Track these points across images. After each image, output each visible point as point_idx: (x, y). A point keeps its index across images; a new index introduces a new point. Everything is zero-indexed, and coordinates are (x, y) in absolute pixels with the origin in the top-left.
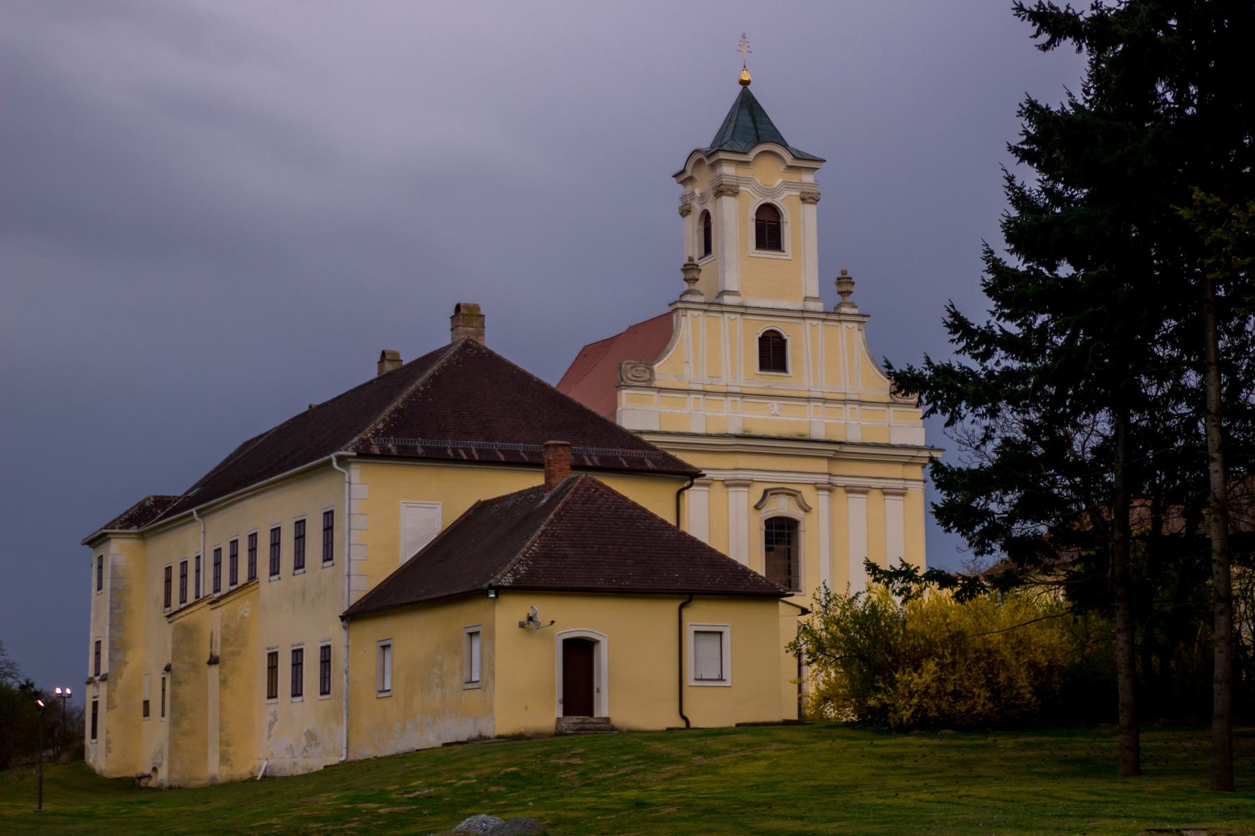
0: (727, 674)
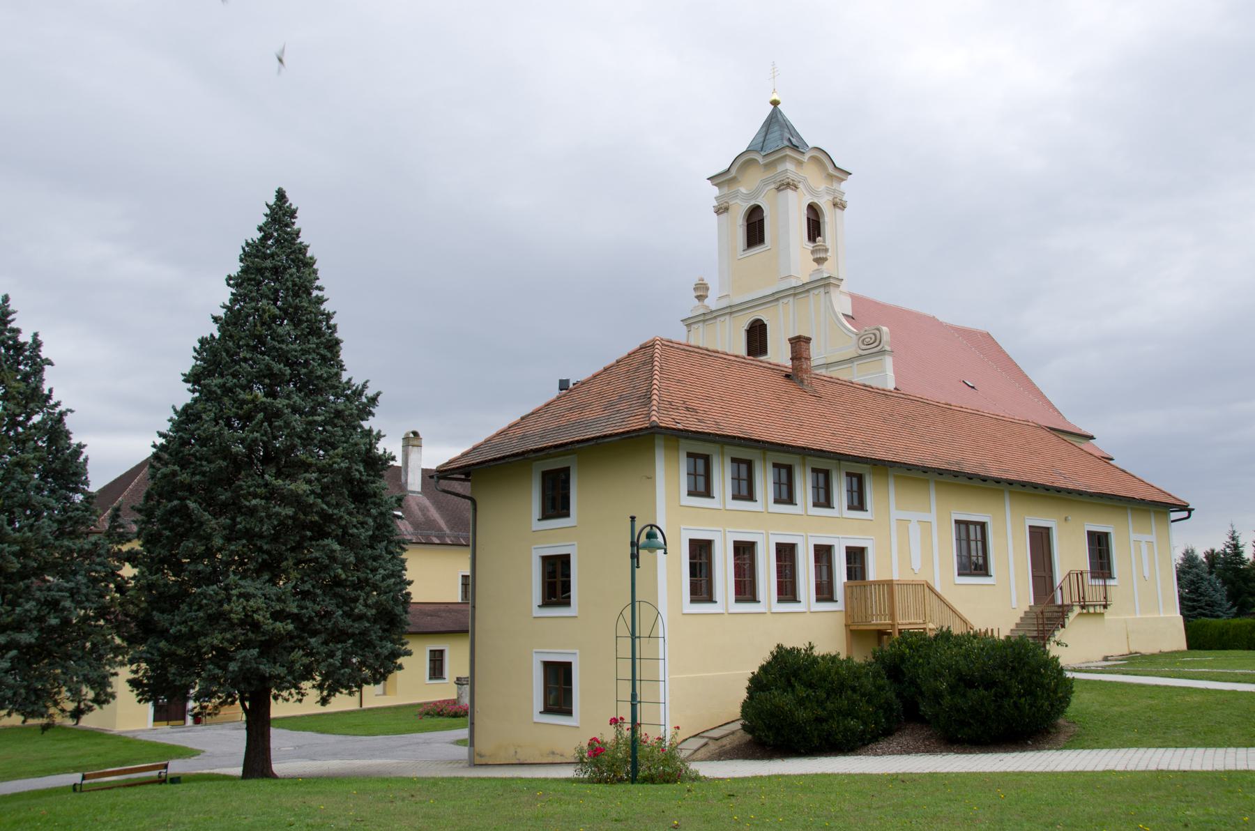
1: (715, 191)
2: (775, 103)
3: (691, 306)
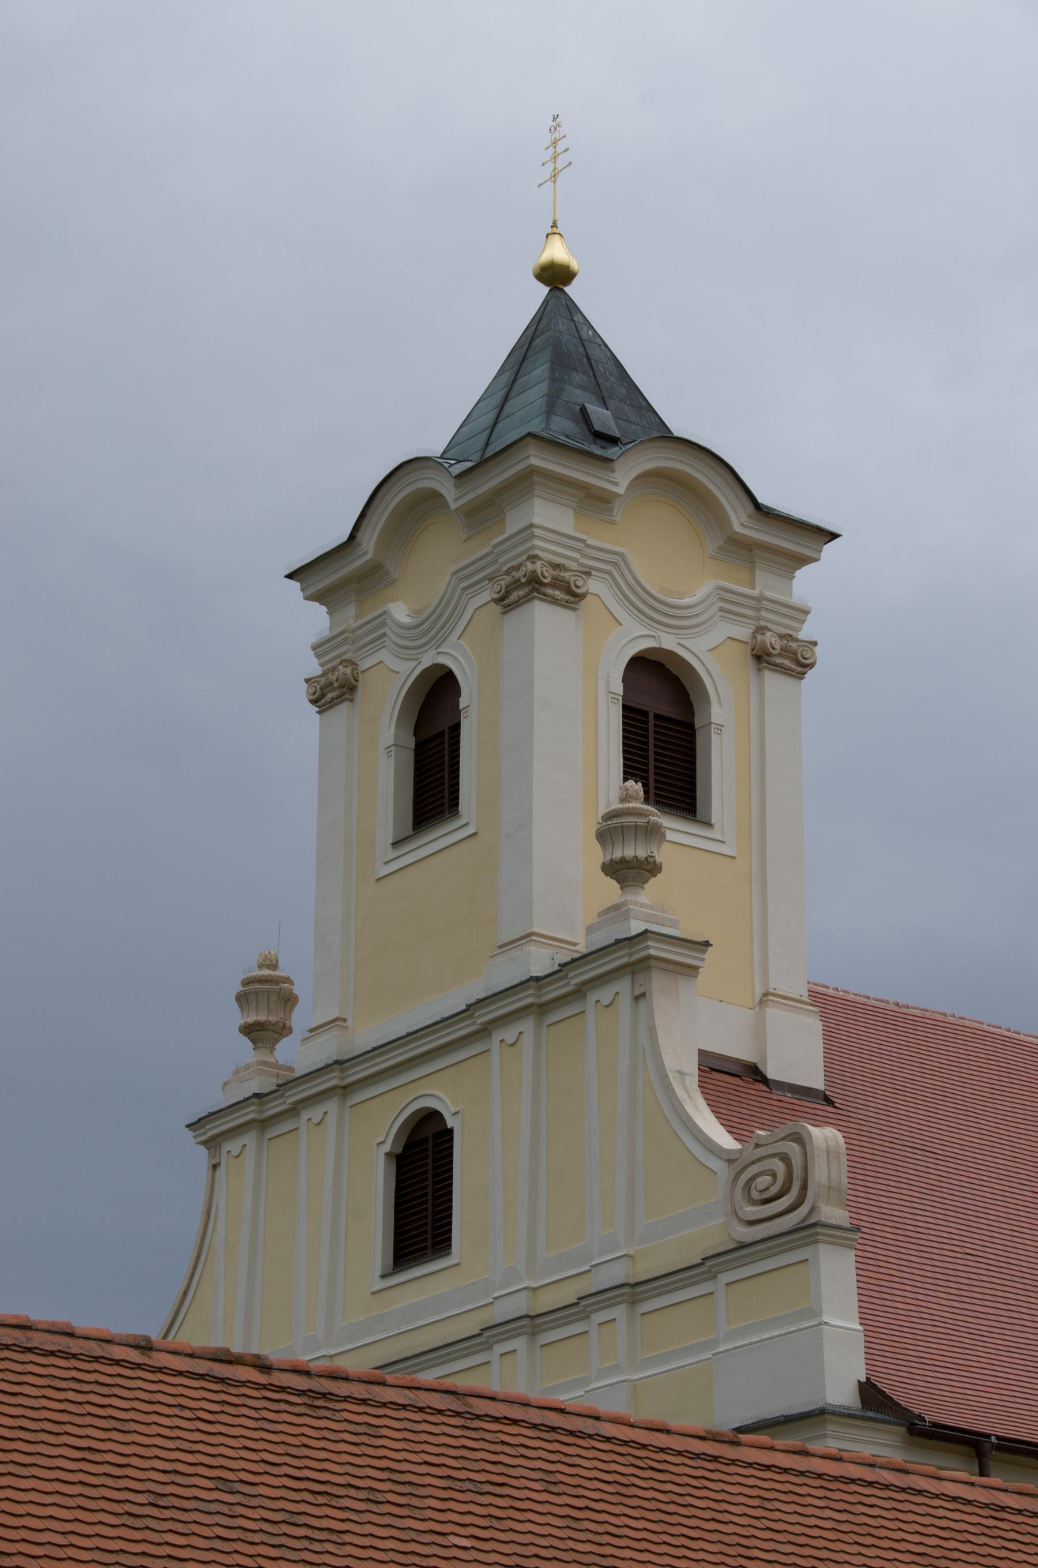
1: (317, 620)
2: (556, 277)
3: (221, 1064)
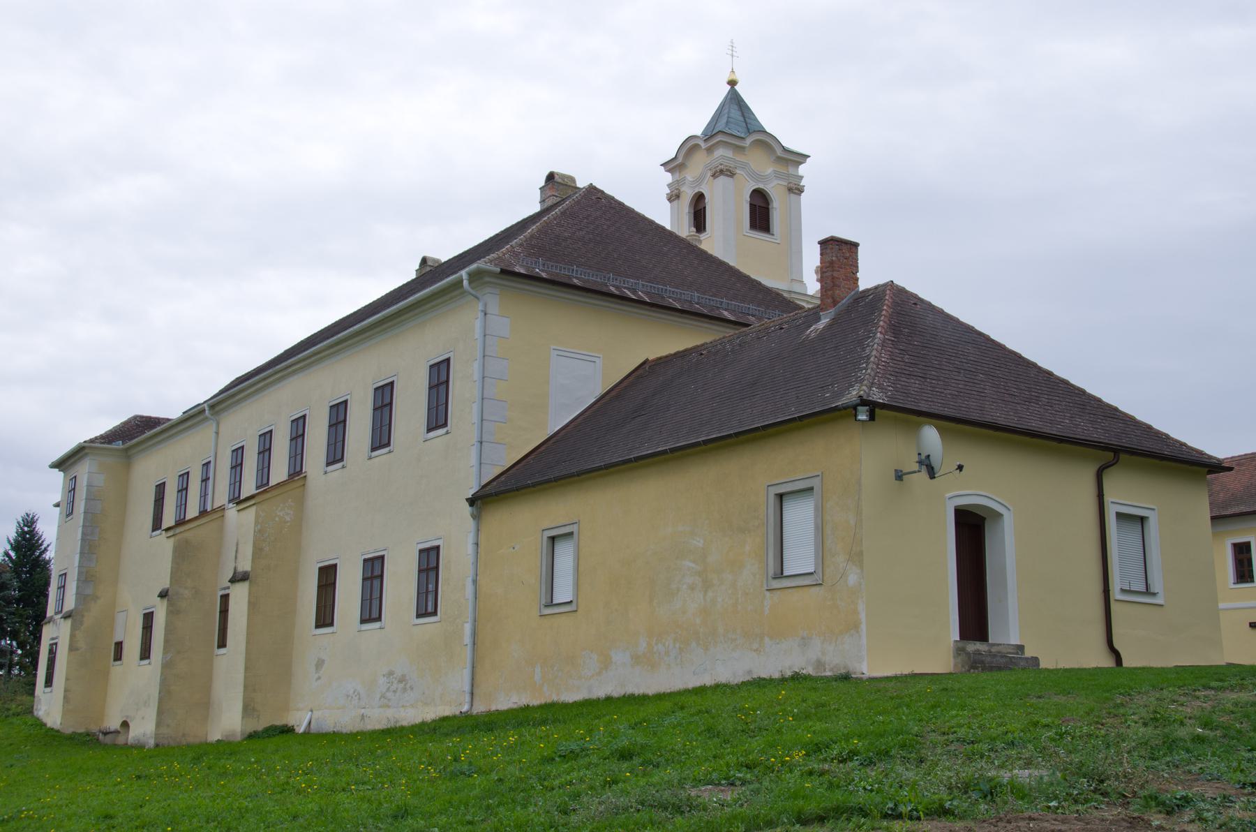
0: (1156, 586)
1: (668, 178)
